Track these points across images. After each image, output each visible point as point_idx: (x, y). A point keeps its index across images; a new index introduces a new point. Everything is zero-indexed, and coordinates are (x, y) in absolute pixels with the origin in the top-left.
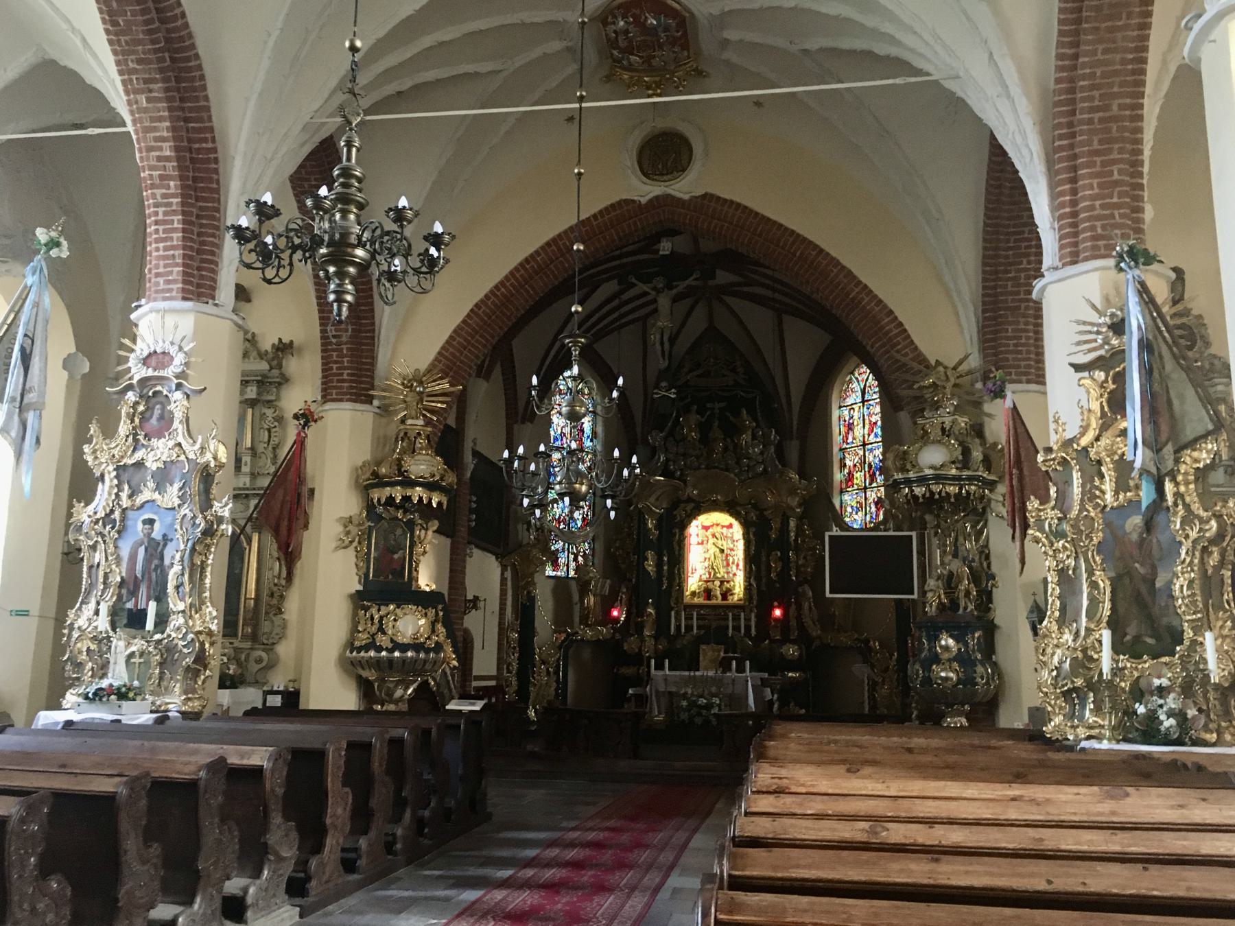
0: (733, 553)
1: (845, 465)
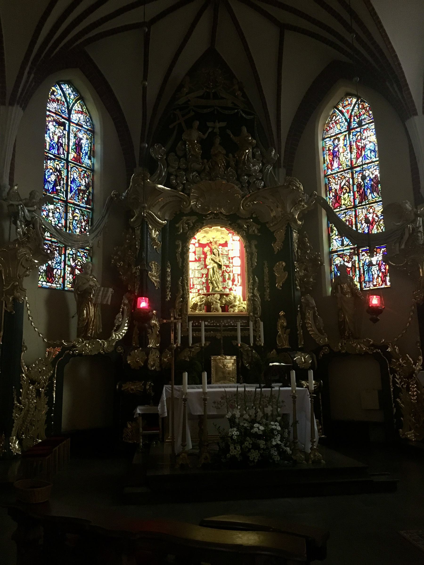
0: (229, 269)
1: (331, 189)
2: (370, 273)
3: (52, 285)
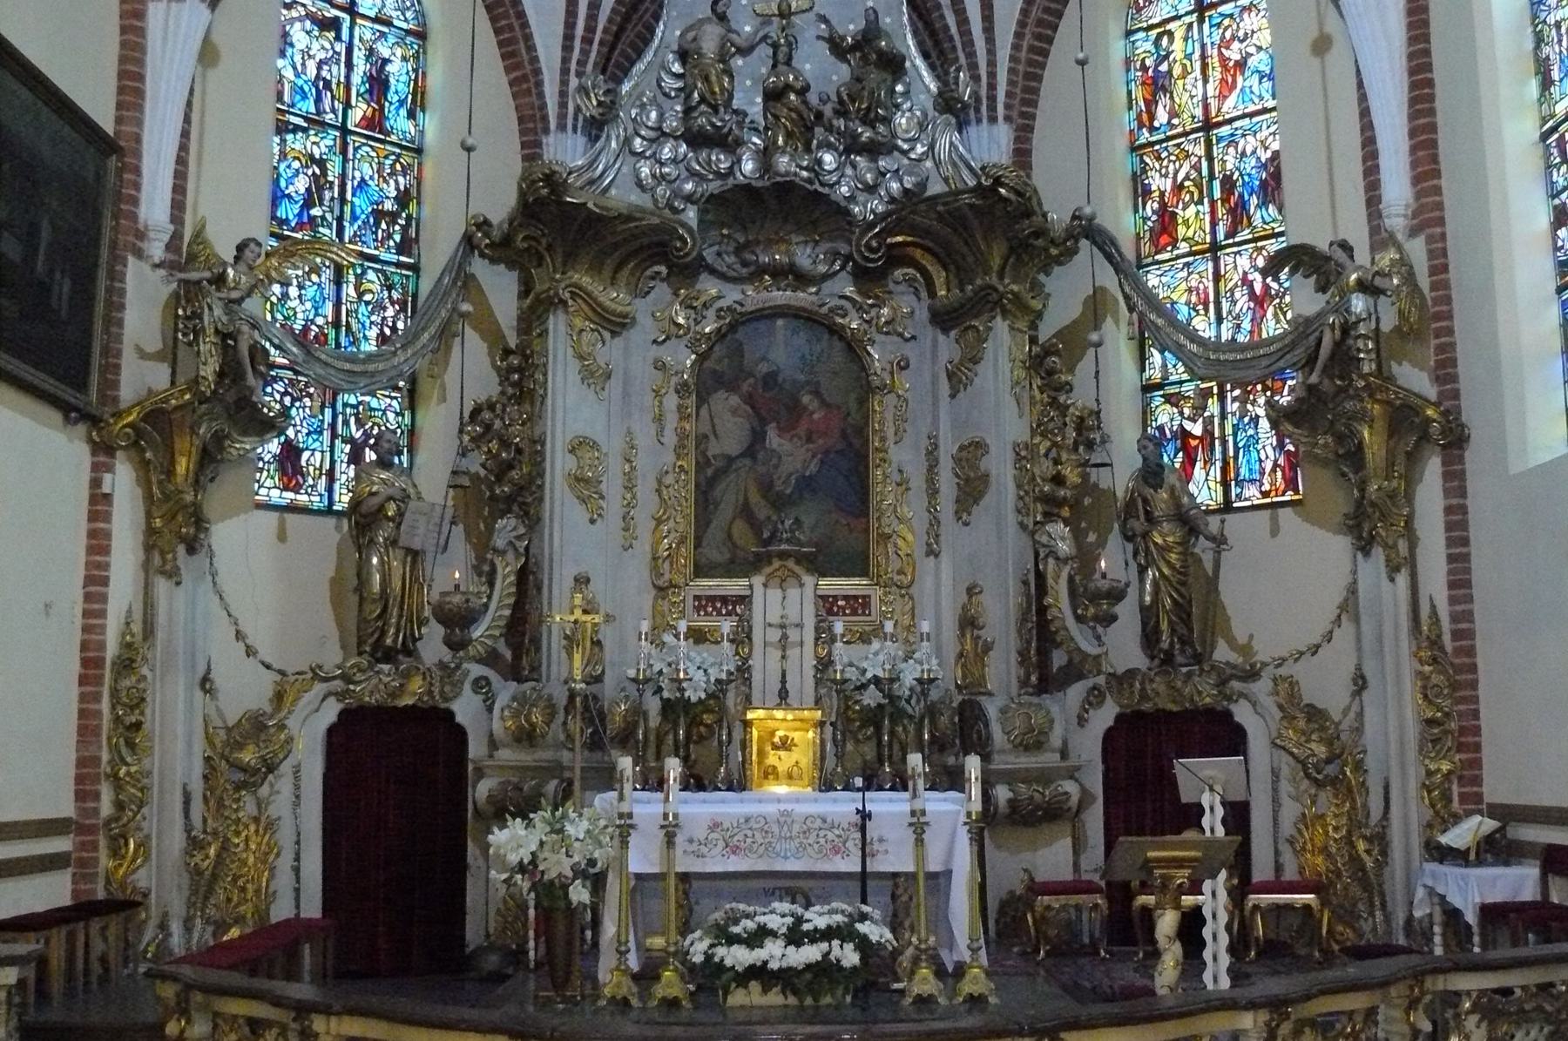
1: (1147, 192)
2: (1254, 455)
3: (299, 497)
